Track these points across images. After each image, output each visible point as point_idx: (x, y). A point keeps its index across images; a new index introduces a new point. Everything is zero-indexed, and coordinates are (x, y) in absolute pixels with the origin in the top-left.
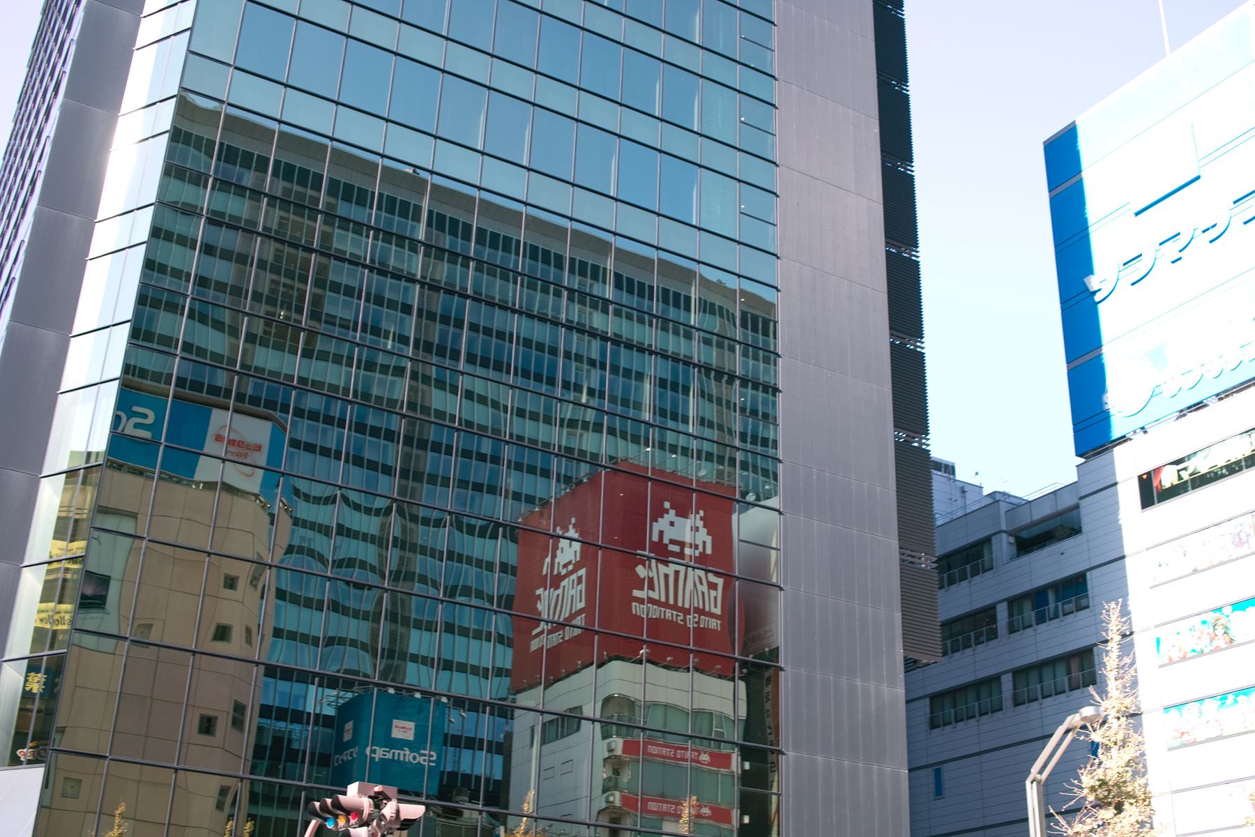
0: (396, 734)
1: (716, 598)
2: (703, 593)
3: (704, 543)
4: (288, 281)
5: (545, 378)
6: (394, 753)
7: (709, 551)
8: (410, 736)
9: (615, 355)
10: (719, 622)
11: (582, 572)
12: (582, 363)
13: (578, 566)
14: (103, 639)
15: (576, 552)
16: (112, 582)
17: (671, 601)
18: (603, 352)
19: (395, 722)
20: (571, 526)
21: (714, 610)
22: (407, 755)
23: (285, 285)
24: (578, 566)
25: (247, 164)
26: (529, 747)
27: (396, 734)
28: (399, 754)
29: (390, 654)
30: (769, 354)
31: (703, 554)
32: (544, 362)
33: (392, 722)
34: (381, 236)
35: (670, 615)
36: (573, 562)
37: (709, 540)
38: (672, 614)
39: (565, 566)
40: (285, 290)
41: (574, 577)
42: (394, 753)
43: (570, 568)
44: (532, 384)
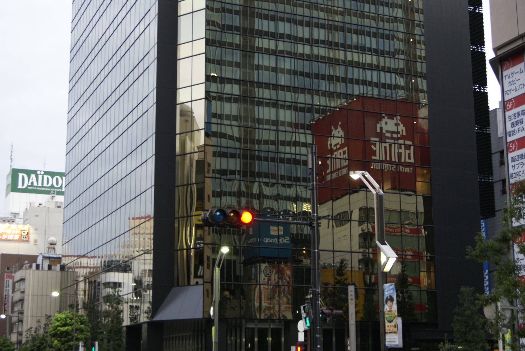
0: (272, 233)
3: (402, 130)
7: (404, 134)
11: (346, 149)
13: (342, 146)
14: (124, 277)
19: (271, 227)
20: (339, 126)
26: (327, 228)
31: (402, 135)
33: (270, 228)
34: (255, 85)
35: (388, 167)
36: (340, 143)
37: (404, 129)
38: (389, 166)
39: (335, 145)
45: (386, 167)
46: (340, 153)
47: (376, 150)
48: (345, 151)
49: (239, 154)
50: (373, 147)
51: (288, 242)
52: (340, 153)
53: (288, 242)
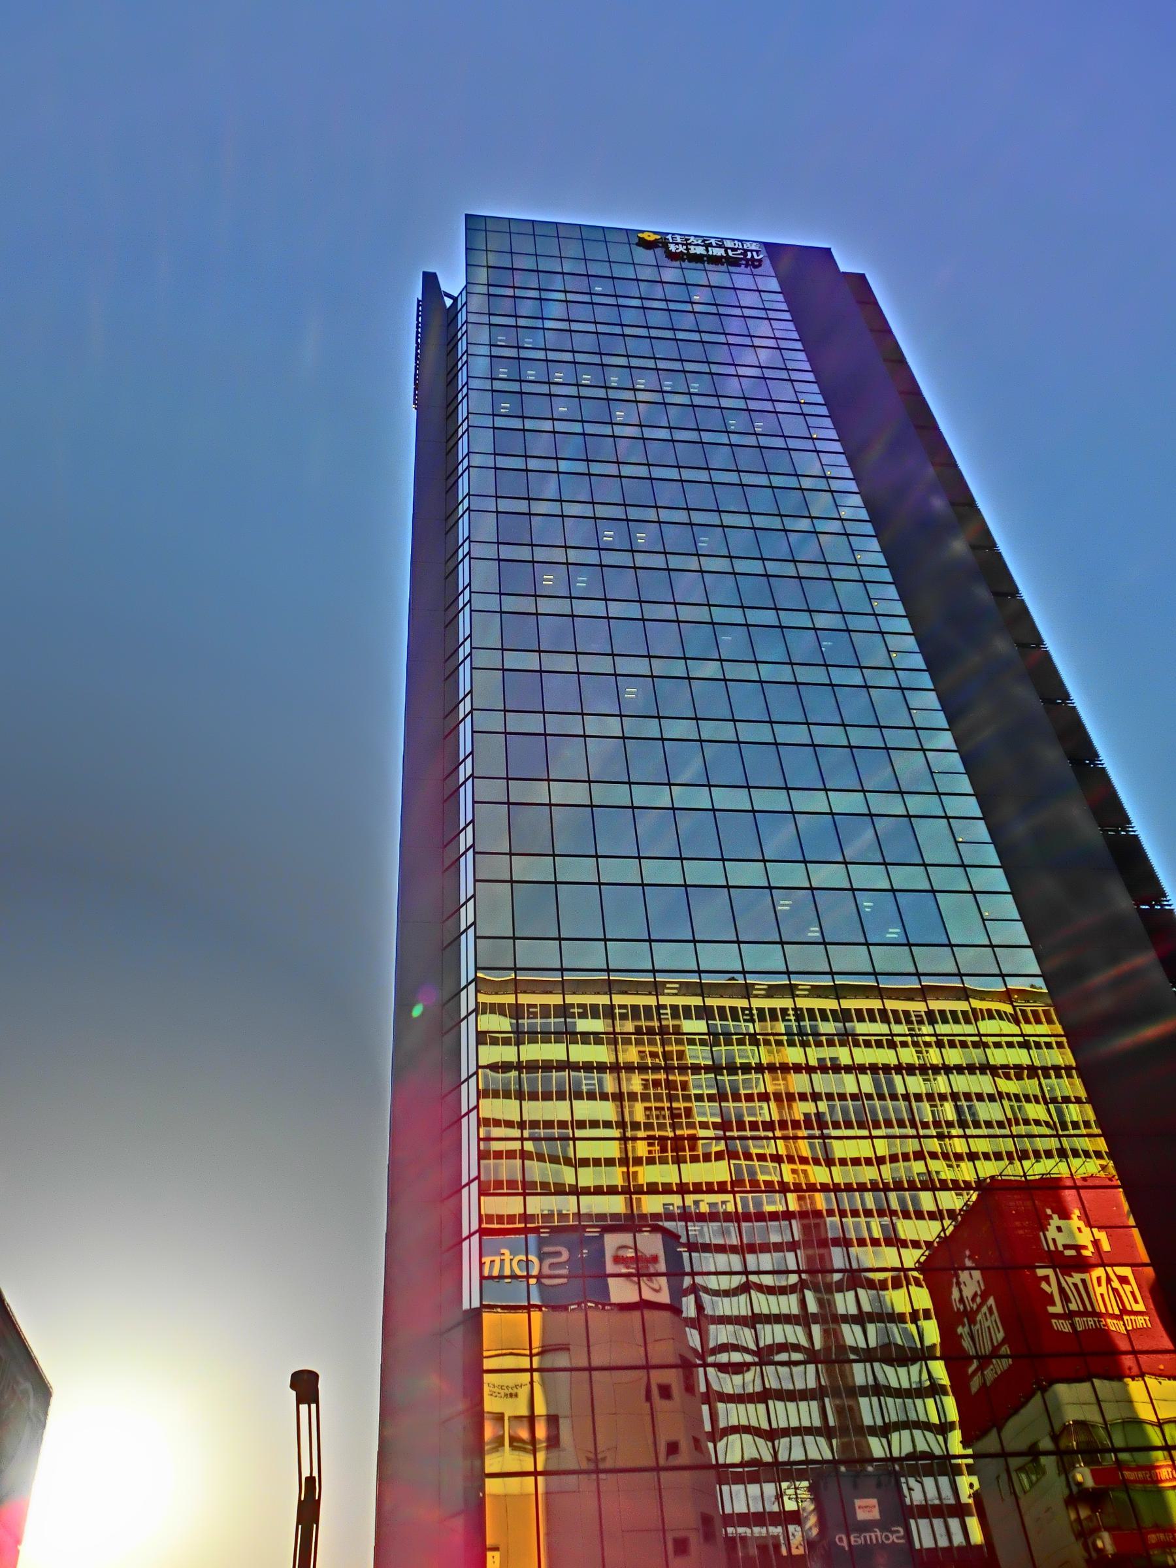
1: (1133, 1293)
2: (1102, 1295)
4: (659, 1105)
5: (842, 1123)
6: (865, 1537)
8: (875, 1514)
9: (891, 1084)
10: (1147, 1318)
11: (991, 1301)
12: (885, 1100)
13: (985, 1297)
15: (978, 1282)
16: (561, 1421)
17: (1089, 1309)
18: (877, 1084)
19: (858, 1502)
21: (1136, 1308)
22: (876, 1535)
23: (656, 1108)
24: (985, 1297)
25: (774, 1018)
27: (861, 1515)
28: (870, 1536)
29: (843, 1430)
30: (768, 1037)
32: (731, 1115)
35: (1092, 1323)
36: (979, 1293)
39: (974, 1299)
40: (658, 1112)
41: (984, 1309)
42: (865, 1537)
43: (978, 1300)
44: (897, 1131)
45: (1090, 1323)
46: (1099, 1279)
47: (1052, 1292)
48: (991, 1306)
49: (944, 1219)
50: (1044, 1285)
51: (902, 1541)
52: (1099, 1279)
53: (902, 1541)
